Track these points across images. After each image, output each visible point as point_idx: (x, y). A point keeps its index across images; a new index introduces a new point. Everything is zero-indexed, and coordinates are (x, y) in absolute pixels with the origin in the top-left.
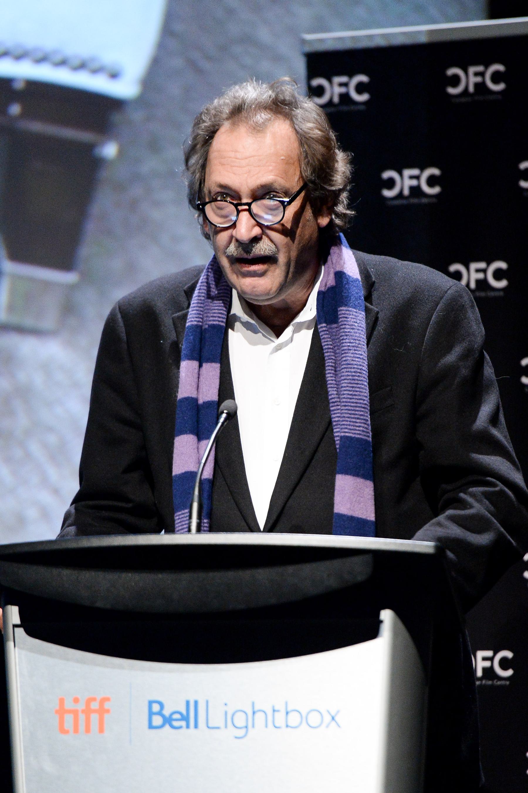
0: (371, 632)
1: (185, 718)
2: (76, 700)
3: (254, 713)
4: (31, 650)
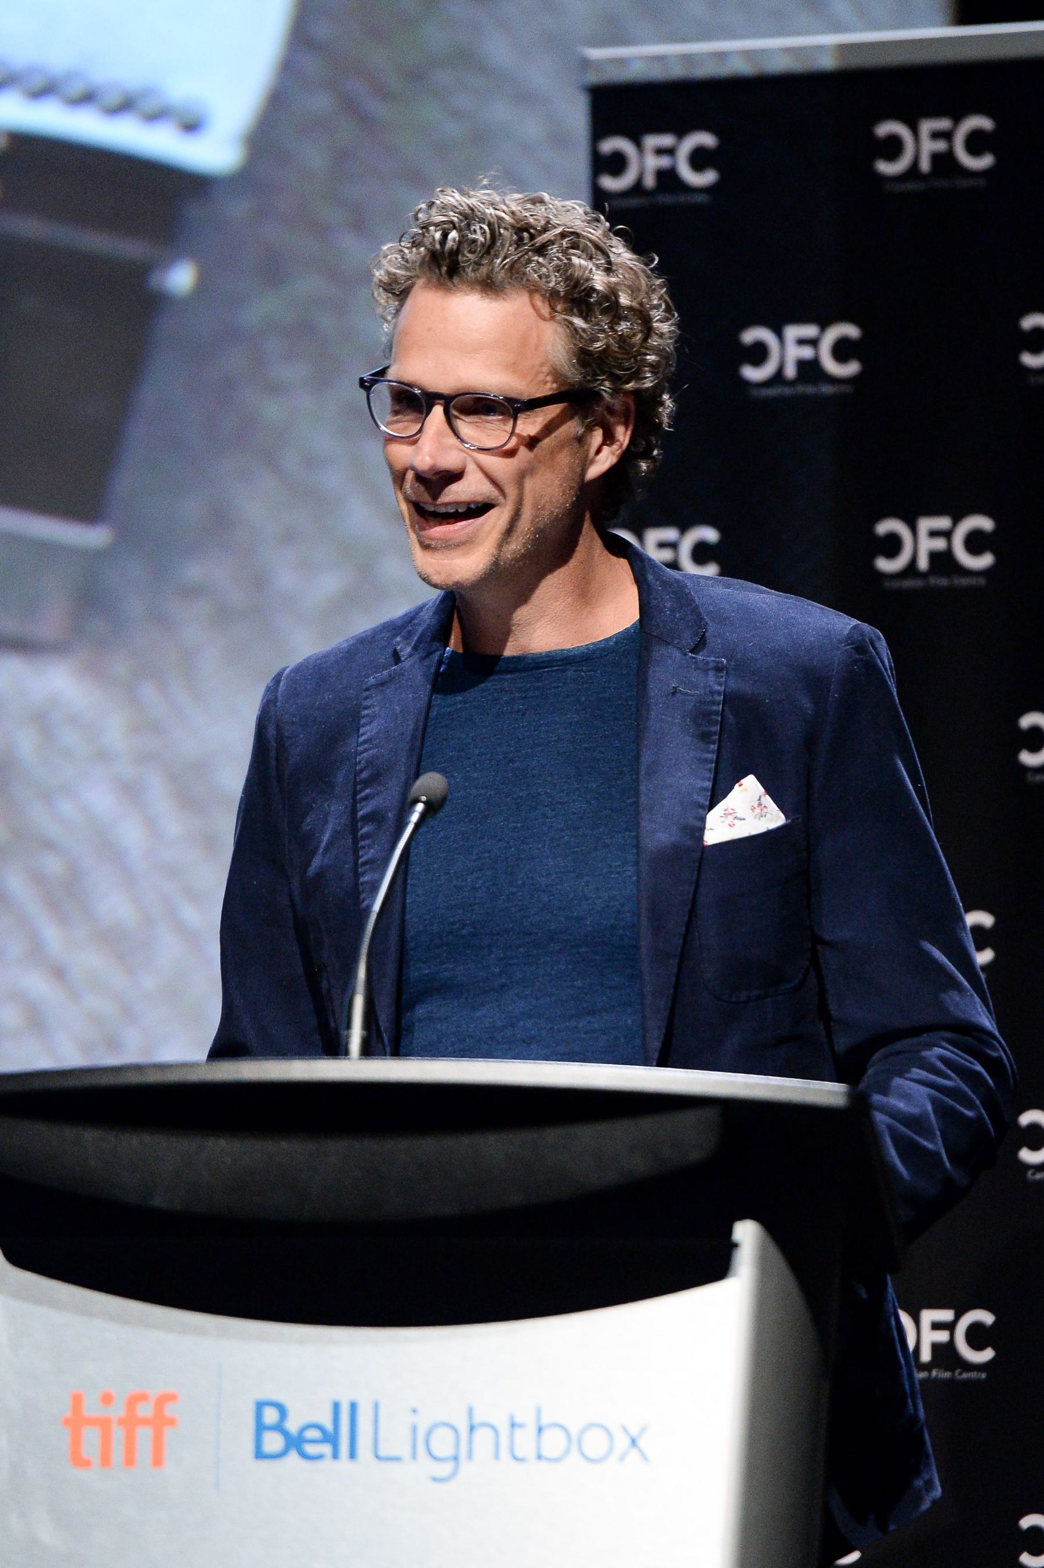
0: (714, 1266)
1: (331, 1438)
2: (107, 1399)
3: (472, 1429)
4: (18, 1294)
